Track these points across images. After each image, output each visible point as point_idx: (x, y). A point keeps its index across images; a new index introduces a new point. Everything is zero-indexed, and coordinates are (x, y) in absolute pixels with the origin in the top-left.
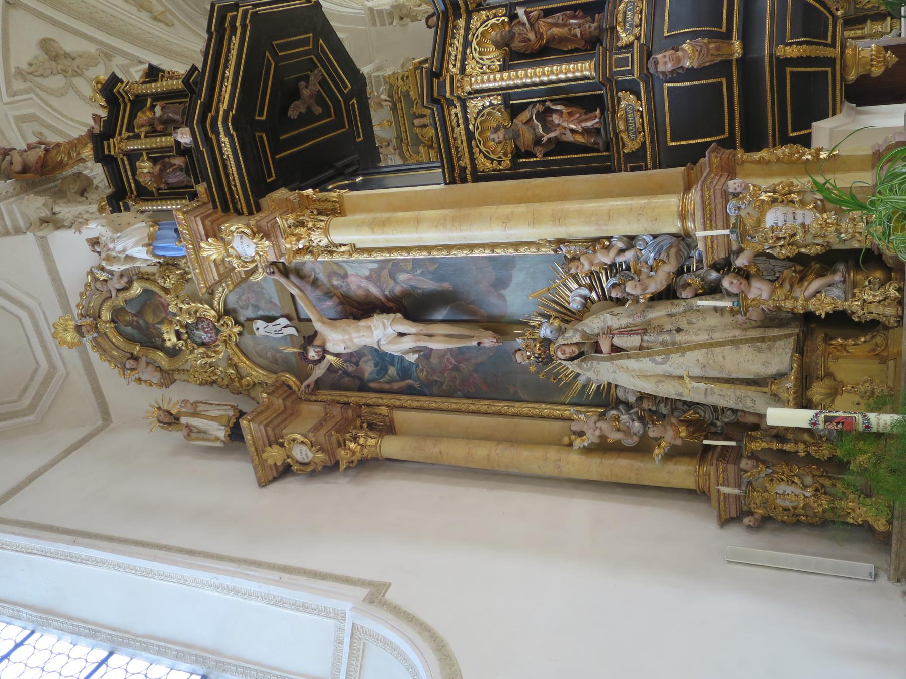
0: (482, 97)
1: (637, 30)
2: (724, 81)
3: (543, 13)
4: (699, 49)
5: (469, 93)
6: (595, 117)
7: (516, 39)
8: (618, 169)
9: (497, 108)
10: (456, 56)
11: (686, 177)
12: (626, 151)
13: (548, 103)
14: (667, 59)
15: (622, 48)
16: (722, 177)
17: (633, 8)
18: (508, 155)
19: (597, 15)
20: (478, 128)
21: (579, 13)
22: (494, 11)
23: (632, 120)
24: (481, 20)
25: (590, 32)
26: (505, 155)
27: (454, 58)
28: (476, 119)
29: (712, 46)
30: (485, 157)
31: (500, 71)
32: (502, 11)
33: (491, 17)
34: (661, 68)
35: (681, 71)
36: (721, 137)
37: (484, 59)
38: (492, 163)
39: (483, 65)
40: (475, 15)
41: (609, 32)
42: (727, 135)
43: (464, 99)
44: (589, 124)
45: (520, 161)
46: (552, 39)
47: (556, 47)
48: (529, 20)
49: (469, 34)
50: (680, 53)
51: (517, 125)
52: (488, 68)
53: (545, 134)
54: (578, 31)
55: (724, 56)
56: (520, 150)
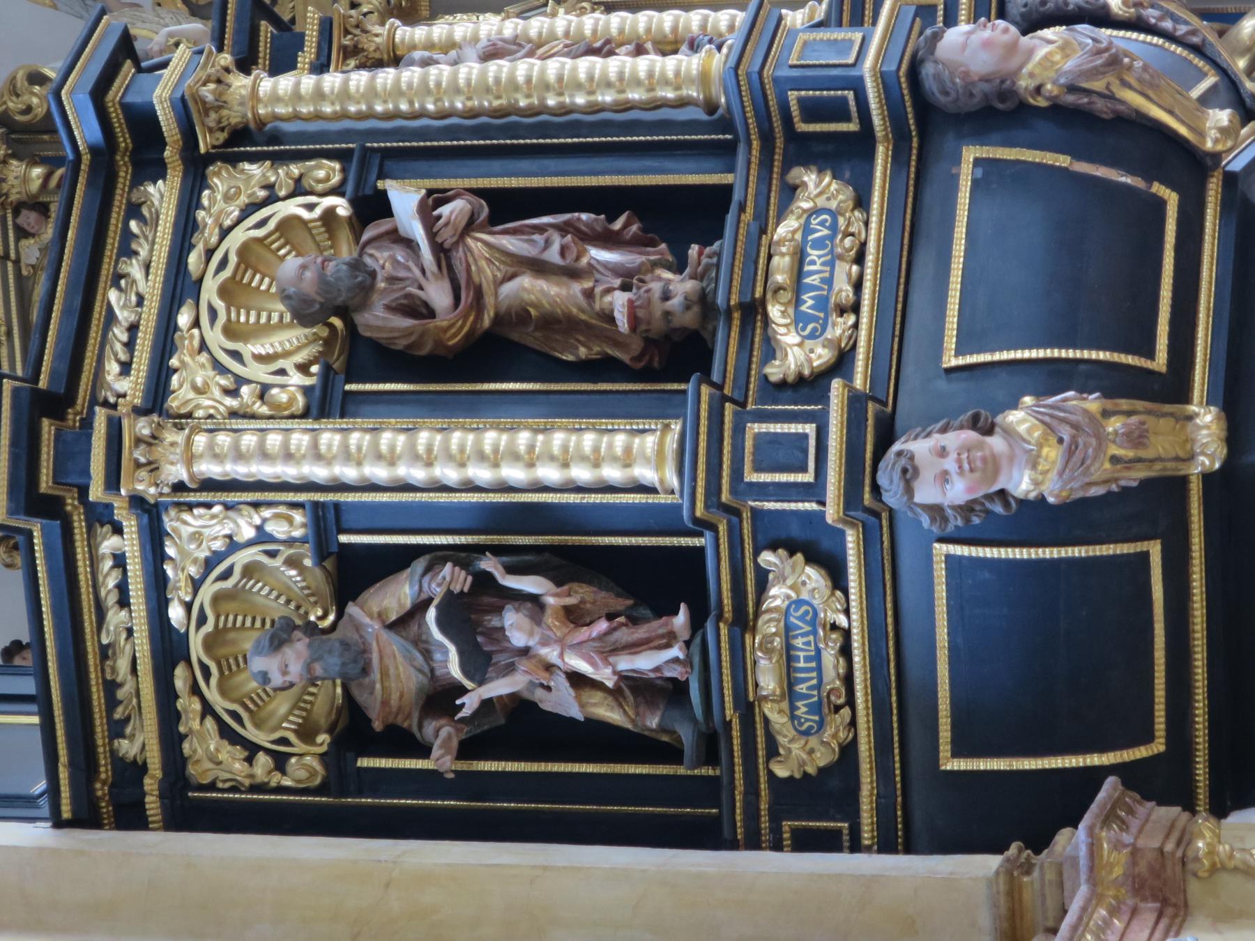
0: (228, 507)
1: (839, 327)
2: (1155, 550)
3: (486, 211)
4: (1066, 435)
5: (179, 487)
6: (669, 639)
7: (375, 297)
8: (746, 833)
9: (287, 552)
10: (133, 329)
11: (1002, 900)
12: (781, 772)
13: (489, 564)
14: (950, 464)
15: (783, 385)
16: (1135, 925)
17: (832, 238)
18: (316, 732)
19: (694, 250)
20: (202, 620)
21: (626, 225)
22: (295, 170)
23: (807, 659)
24: (243, 199)
25: (667, 314)
26: (307, 733)
27: (124, 337)
28: (196, 585)
29: (1115, 425)
30: (227, 733)
31: (305, 415)
32: (327, 171)
33: (282, 193)
34: (926, 493)
35: (998, 509)
36: (1141, 752)
37: (247, 357)
38: (250, 760)
39: (240, 381)
40: (218, 174)
41: (736, 322)
42: (1159, 746)
43: (157, 505)
44: (645, 662)
45: (364, 762)
46: (519, 316)
47: (530, 342)
48: (432, 235)
49: (191, 247)
50: (996, 443)
51: (358, 627)
52: (262, 397)
53: (468, 684)
54: (619, 301)
55: (1158, 466)
56: (369, 721)
